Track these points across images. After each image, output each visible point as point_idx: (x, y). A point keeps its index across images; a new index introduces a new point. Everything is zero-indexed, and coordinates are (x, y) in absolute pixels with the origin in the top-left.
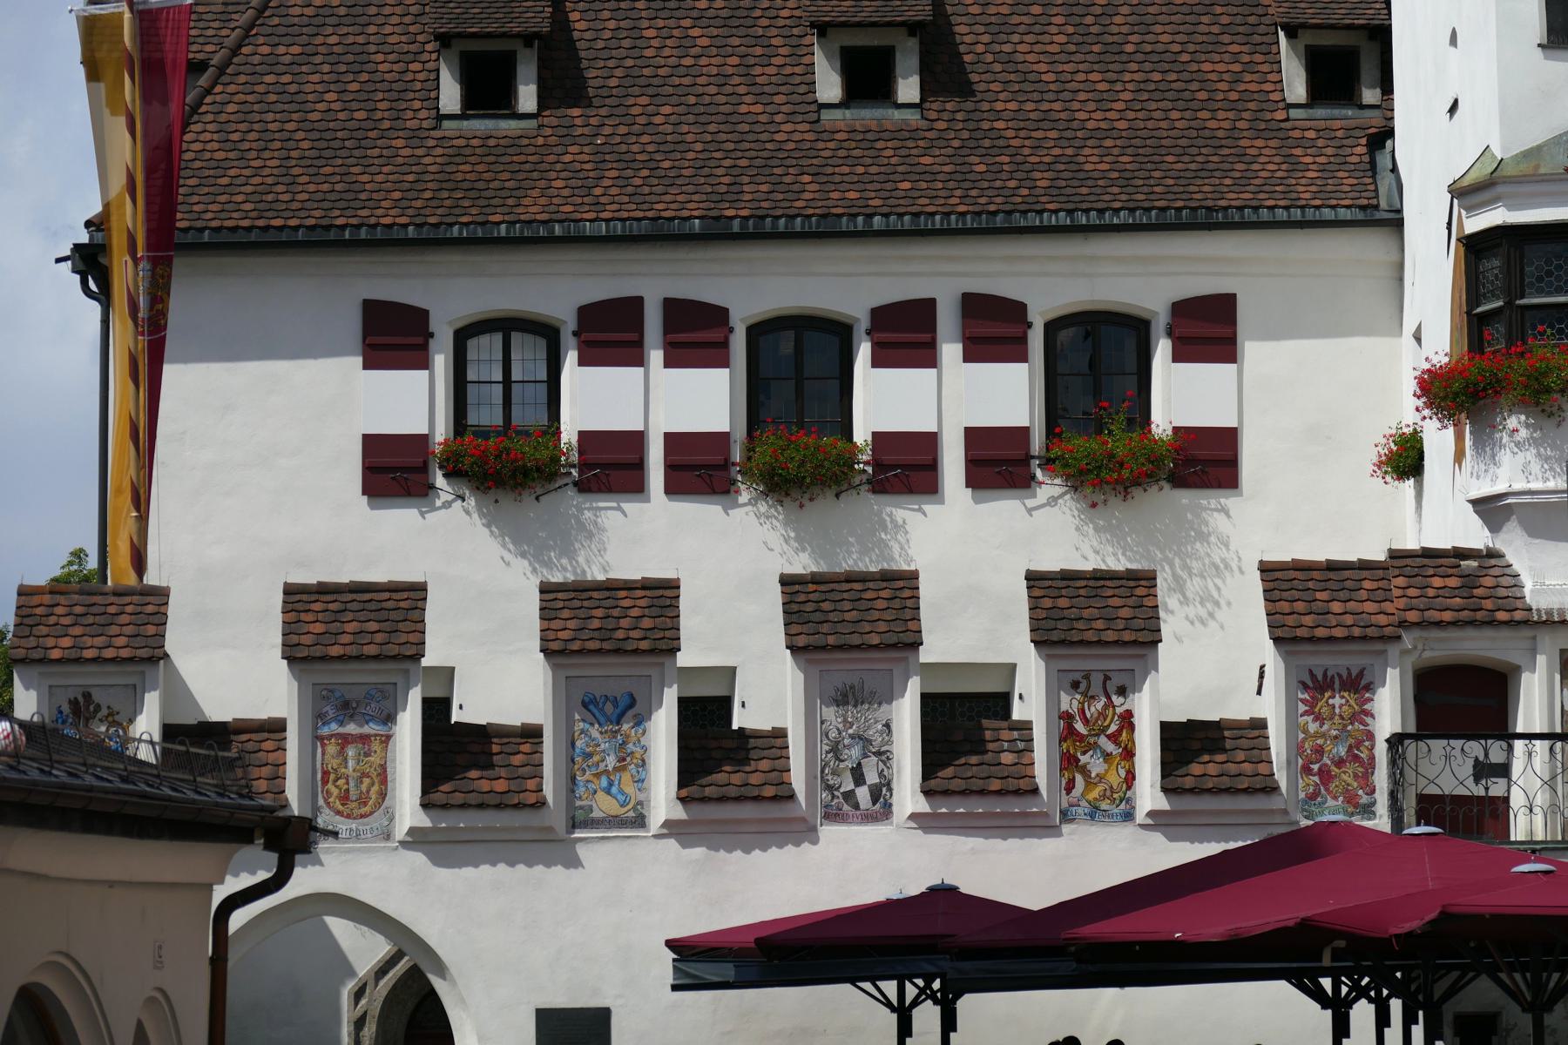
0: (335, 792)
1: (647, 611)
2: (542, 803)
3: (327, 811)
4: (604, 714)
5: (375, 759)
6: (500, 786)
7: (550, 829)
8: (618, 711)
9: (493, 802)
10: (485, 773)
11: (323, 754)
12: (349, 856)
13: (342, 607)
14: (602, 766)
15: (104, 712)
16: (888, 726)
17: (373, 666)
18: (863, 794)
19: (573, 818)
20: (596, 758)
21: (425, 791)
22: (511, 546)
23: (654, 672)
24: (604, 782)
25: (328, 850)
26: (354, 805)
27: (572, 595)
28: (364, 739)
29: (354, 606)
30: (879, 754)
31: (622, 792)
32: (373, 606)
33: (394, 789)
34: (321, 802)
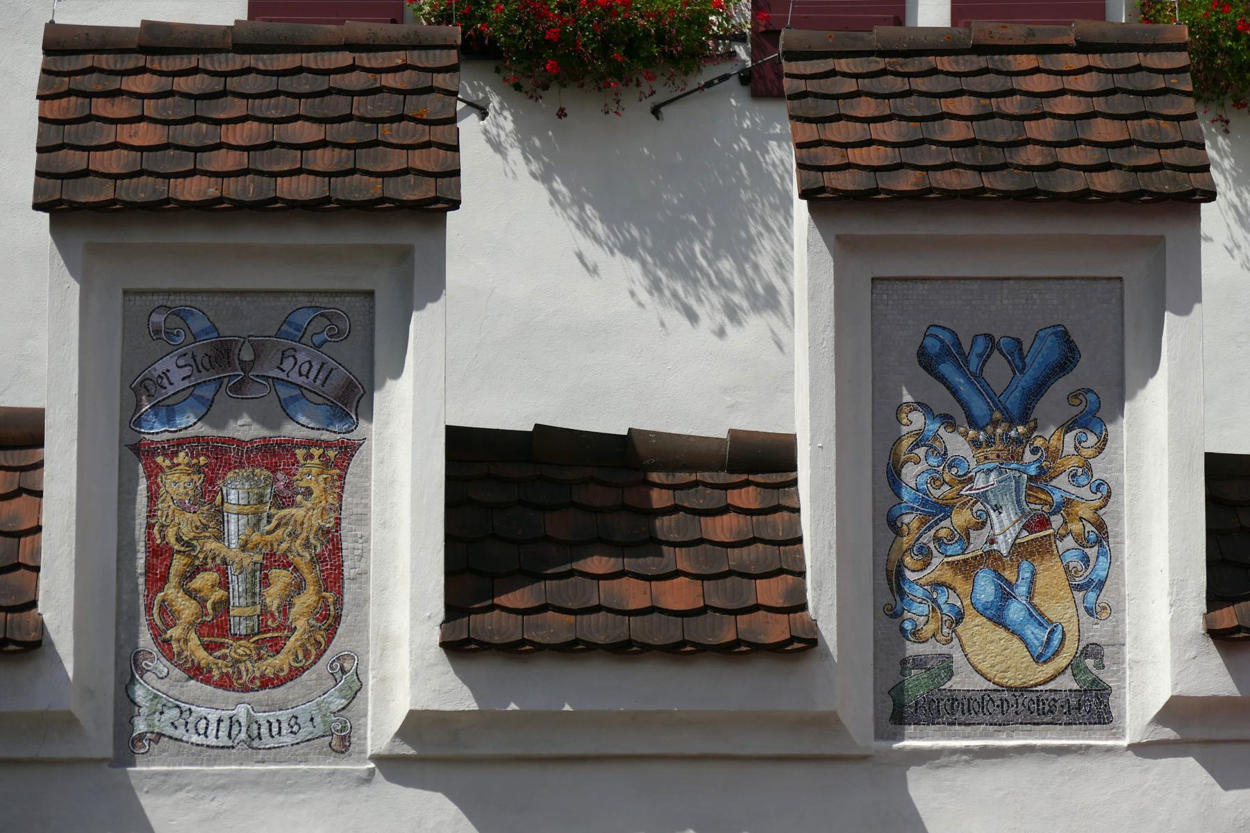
0: (187, 609)
1: (1099, 104)
2: (805, 644)
3: (163, 666)
4: (985, 391)
5: (306, 514)
6: (679, 595)
7: (828, 723)
8: (1026, 380)
9: (658, 640)
10: (630, 563)
11: (153, 498)
12: (227, 801)
13: (216, 85)
14: (978, 542)
17: (307, 236)
19: (897, 693)
20: (961, 518)
21: (457, 605)
22: (600, 228)
23: (1133, 269)
24: (985, 588)
25: (166, 783)
26: (241, 649)
27: (881, 63)
28: (275, 455)
29: (252, 84)
31: (1037, 615)
32: (304, 83)
33: (362, 603)
34: (145, 639)
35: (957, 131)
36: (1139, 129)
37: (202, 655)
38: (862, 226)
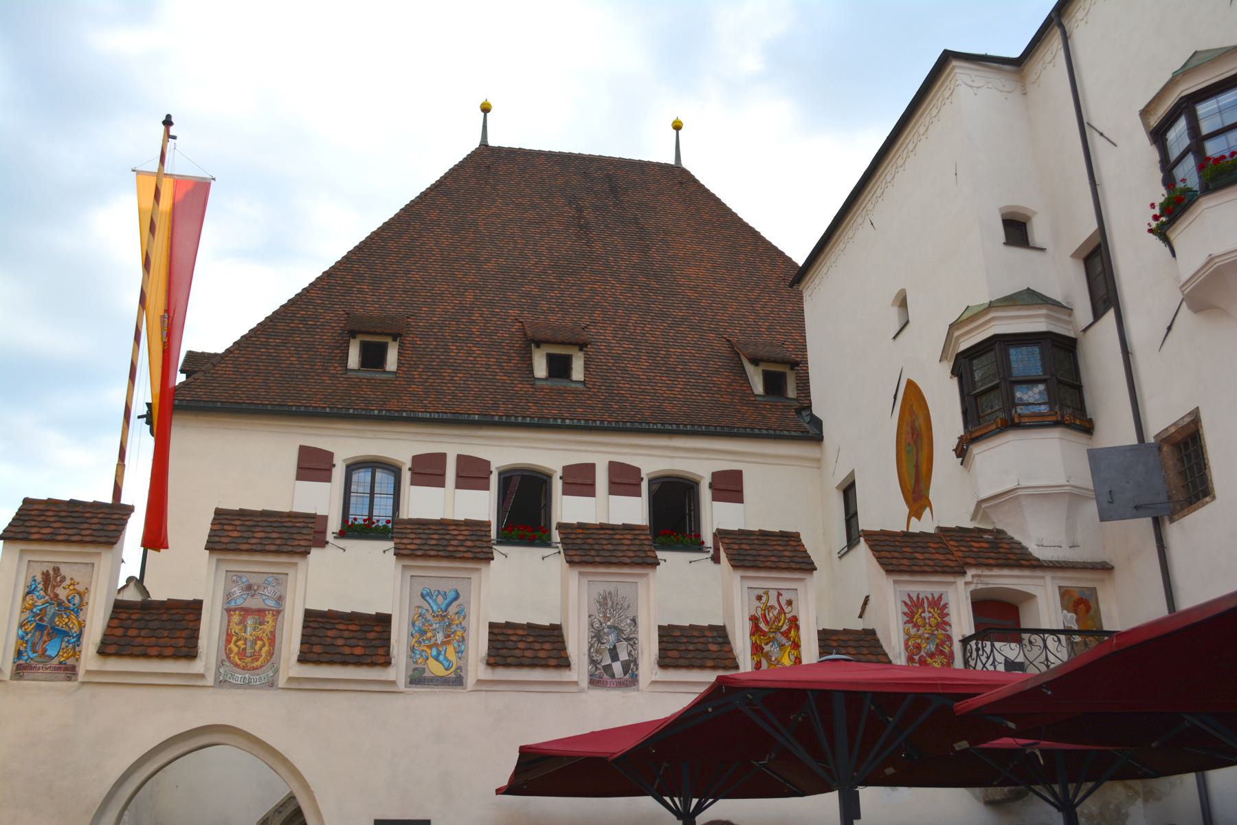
0: (235, 649)
5: (267, 628)
8: (447, 602)
15: (68, 582)
16: (634, 621)
18: (617, 668)
20: (429, 634)
24: (434, 652)
26: (248, 660)
30: (628, 639)
31: (446, 659)
35: (434, 542)
36: (477, 543)
37: (238, 662)
38: (408, 562)
